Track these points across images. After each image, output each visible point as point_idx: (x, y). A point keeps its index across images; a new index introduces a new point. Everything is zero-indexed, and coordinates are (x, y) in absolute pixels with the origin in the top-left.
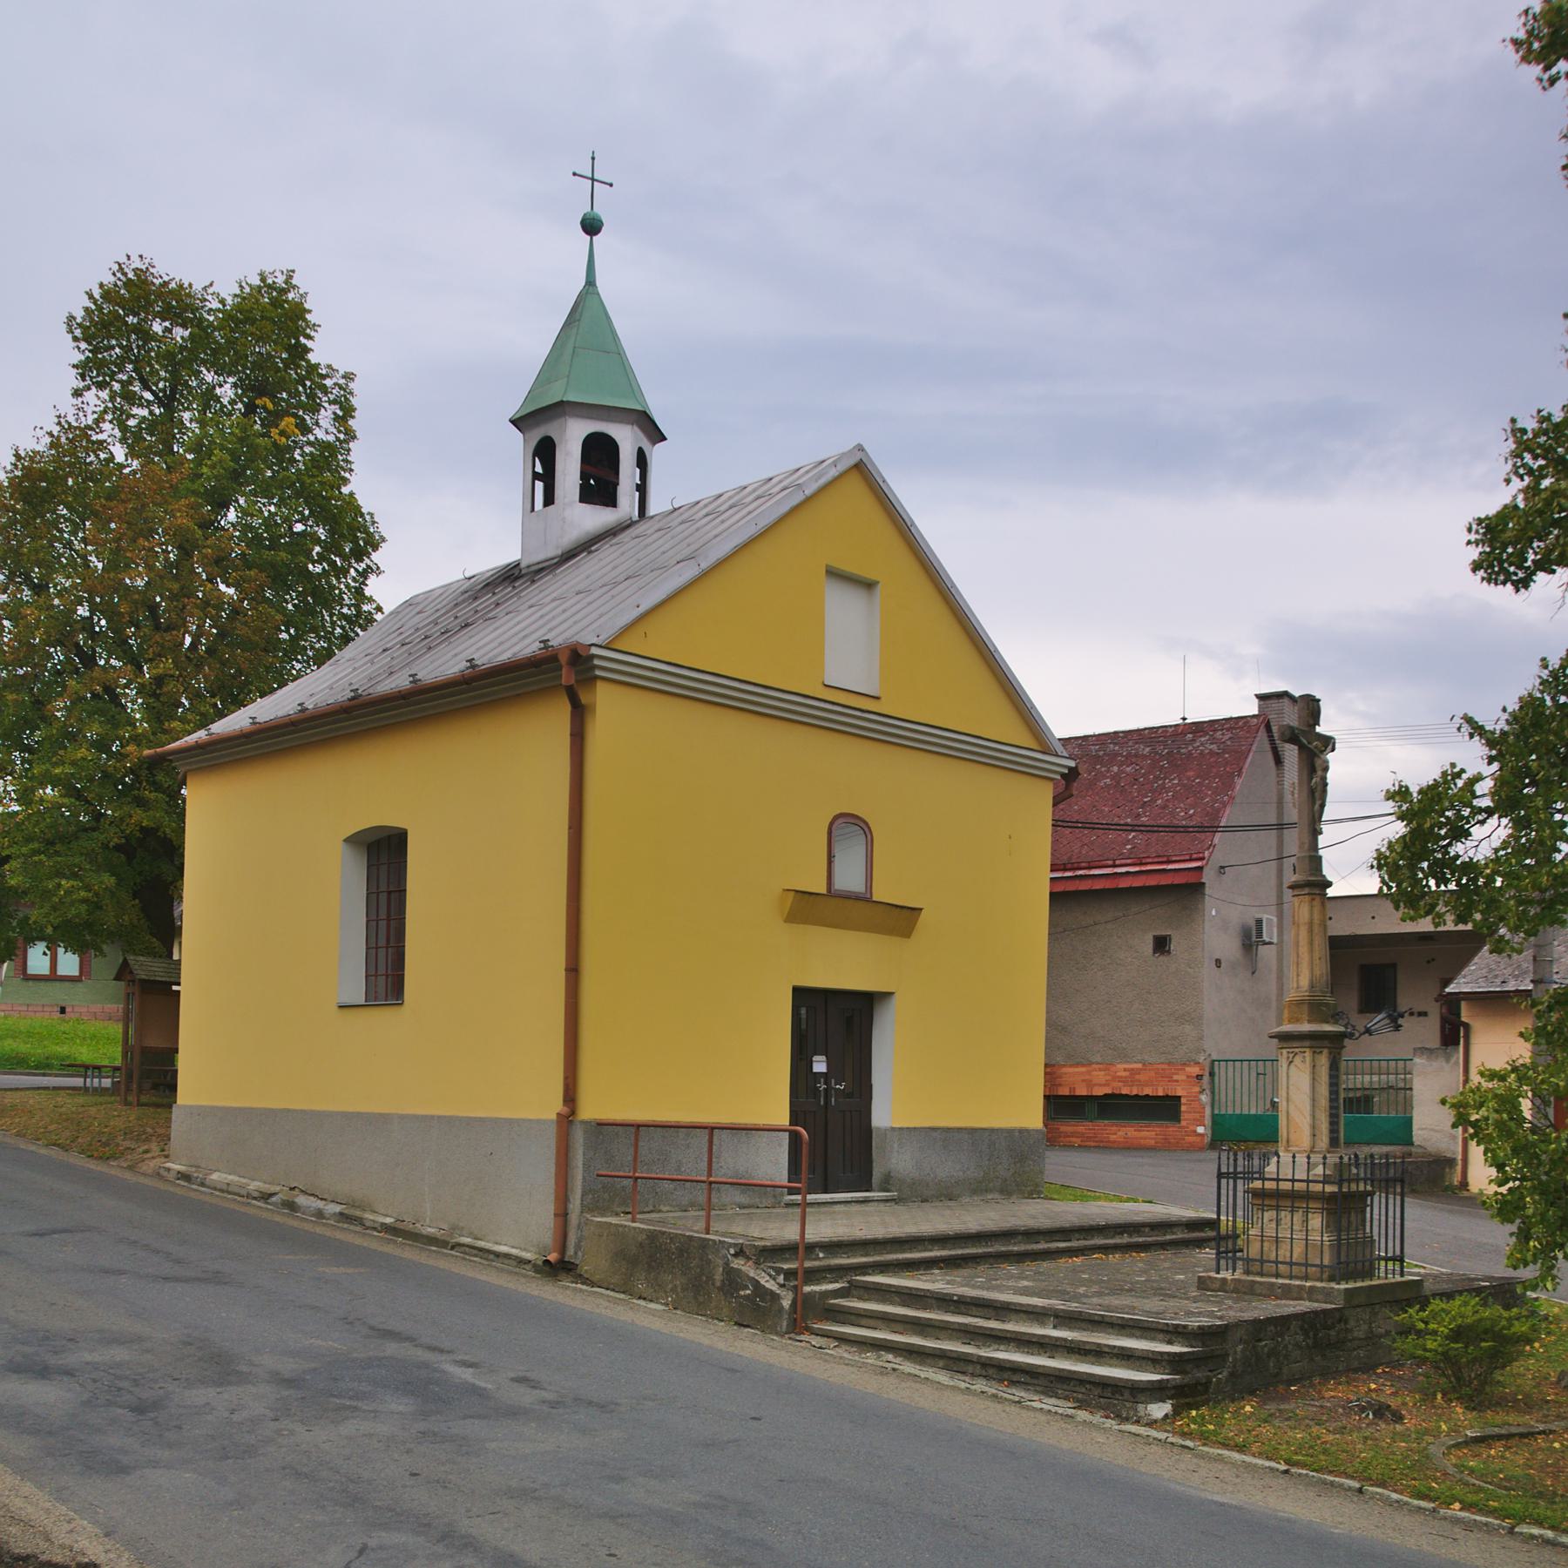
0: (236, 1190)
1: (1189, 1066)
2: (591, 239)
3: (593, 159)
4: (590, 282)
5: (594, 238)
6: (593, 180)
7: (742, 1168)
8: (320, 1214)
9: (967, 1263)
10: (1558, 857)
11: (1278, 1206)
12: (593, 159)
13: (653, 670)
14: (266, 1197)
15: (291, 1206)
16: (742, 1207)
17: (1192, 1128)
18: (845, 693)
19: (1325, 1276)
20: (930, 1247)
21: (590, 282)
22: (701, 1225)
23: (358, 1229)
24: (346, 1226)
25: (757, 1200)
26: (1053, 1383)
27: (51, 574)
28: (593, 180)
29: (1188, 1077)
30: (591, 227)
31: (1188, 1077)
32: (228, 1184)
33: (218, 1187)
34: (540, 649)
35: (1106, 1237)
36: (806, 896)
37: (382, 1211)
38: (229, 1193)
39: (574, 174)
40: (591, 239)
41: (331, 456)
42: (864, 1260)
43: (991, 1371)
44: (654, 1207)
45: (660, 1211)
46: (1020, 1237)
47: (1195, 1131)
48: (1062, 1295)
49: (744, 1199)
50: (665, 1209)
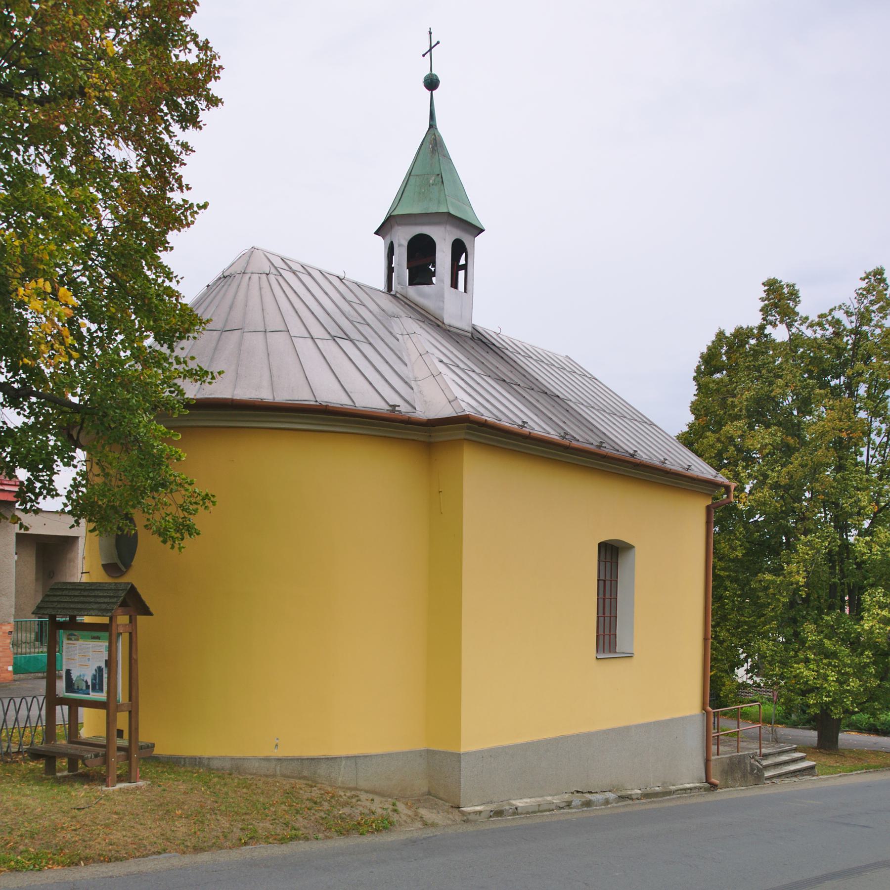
0: (546, 807)
1: (4, 625)
2: (432, 94)
3: (430, 33)
4: (432, 126)
5: (434, 92)
8: (607, 802)
10: (888, 296)
12: (430, 33)
14: (569, 805)
15: (588, 804)
17: (5, 667)
18: (310, 390)
21: (432, 126)
22: (762, 731)
23: (630, 802)
24: (655, 799)
26: (795, 773)
29: (4, 633)
31: (4, 633)
32: (539, 805)
33: (530, 811)
34: (388, 410)
37: (630, 787)
38: (541, 812)
40: (432, 94)
41: (178, 338)
43: (789, 775)
47: (7, 670)
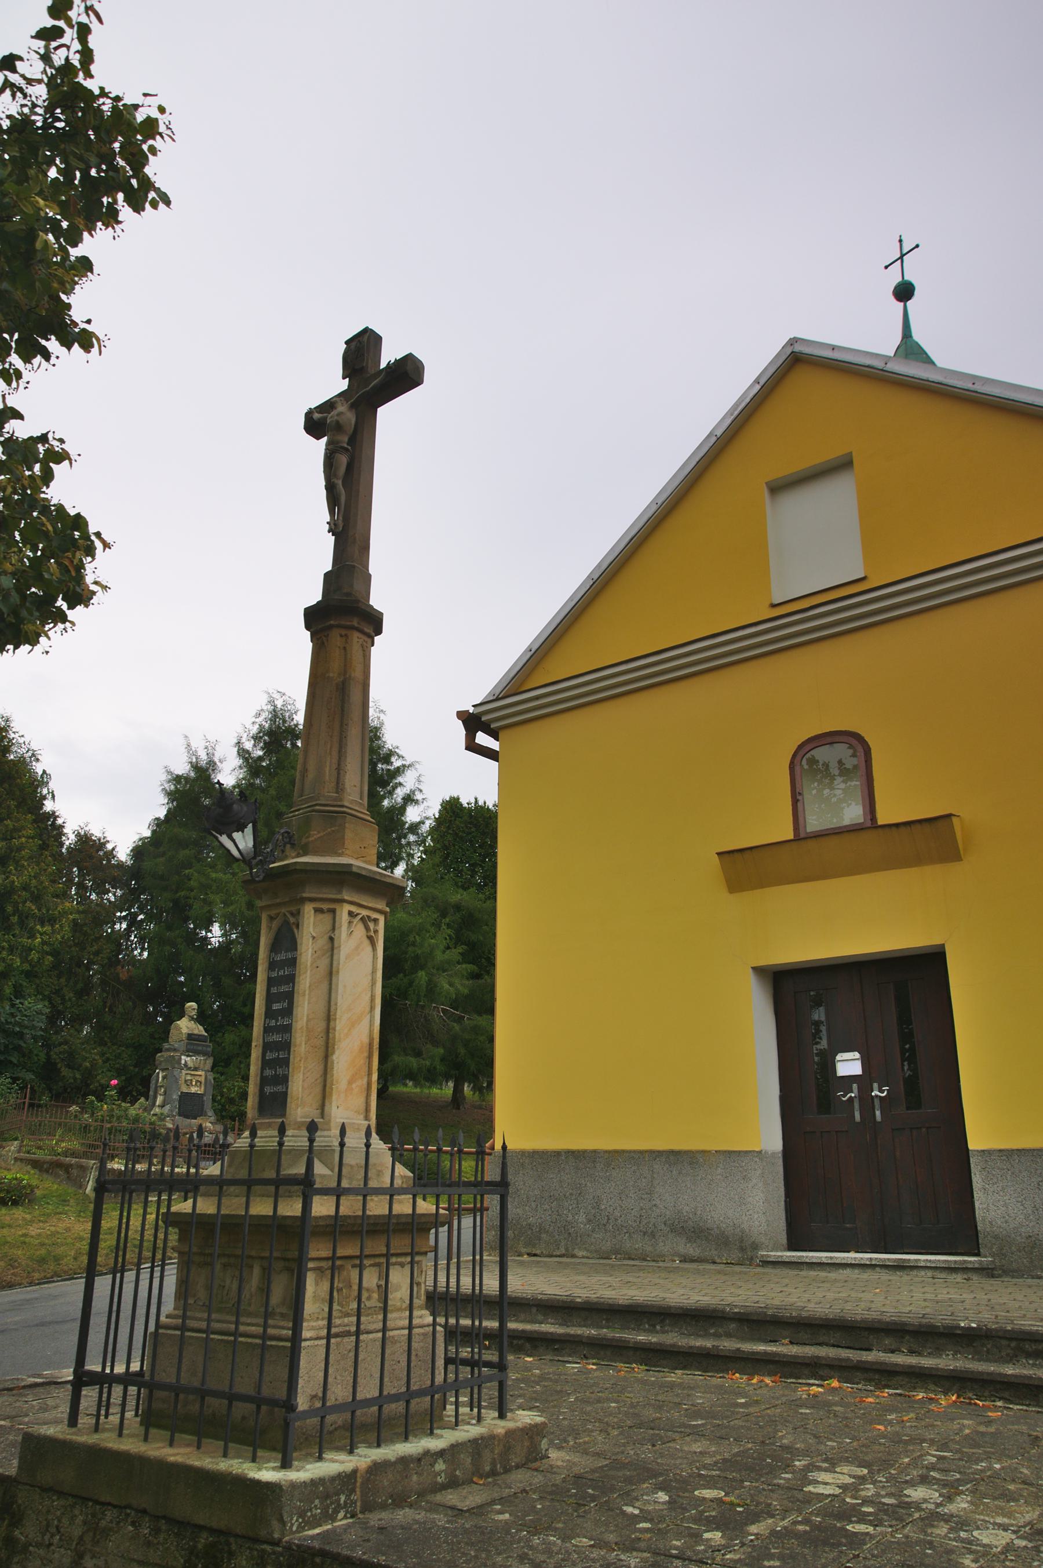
5: (909, 303)
6: (901, 258)
7: (687, 1208)
9: (535, 1347)
11: (387, 1256)
12: (900, 241)
13: (537, 698)
16: (685, 1259)
19: (349, 1515)
20: (540, 1317)
25: (714, 1252)
27: (201, 852)
28: (901, 258)
30: (904, 292)
35: (979, 1357)
36: (737, 855)
39: (886, 267)
42: (795, 1350)
44: (567, 1249)
45: (573, 1256)
46: (733, 1326)
48: (39, 1376)
49: (692, 1250)
50: (580, 1254)
